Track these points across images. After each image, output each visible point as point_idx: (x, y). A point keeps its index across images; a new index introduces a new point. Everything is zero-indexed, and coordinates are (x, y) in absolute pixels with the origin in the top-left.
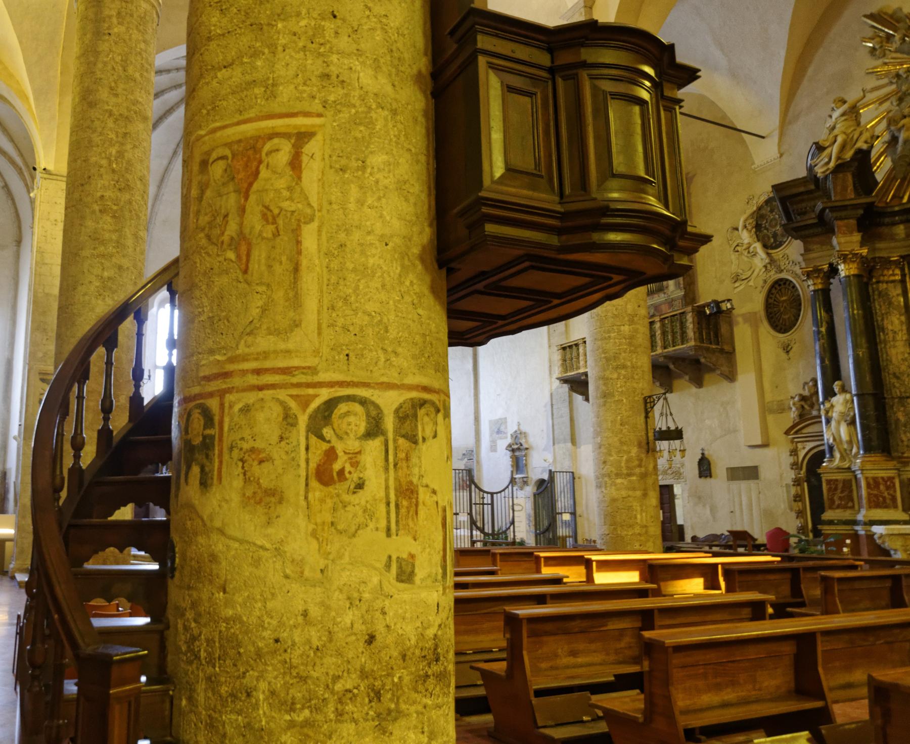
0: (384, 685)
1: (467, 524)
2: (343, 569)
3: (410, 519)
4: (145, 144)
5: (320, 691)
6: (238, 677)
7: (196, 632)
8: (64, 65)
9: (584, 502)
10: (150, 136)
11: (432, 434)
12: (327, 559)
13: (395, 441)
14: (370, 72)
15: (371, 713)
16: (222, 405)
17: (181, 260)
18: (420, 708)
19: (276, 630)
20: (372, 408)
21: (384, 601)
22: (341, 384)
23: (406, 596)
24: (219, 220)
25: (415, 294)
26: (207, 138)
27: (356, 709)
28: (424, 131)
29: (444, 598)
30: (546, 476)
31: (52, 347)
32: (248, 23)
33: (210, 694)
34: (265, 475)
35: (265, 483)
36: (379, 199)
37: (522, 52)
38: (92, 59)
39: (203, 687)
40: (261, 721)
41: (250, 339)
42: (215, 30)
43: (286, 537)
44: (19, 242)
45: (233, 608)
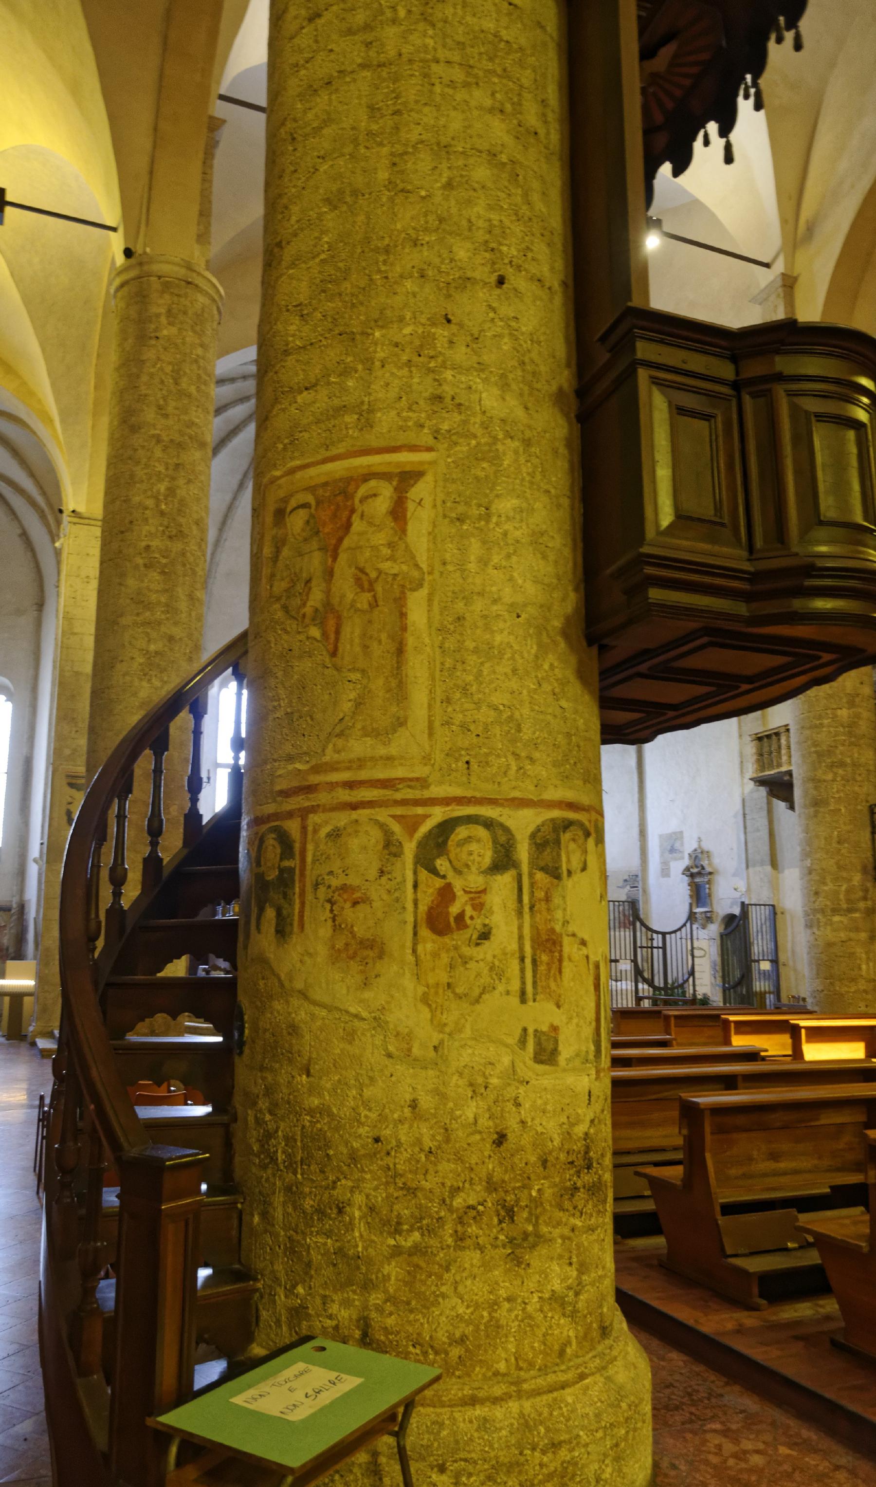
0: (517, 1201)
1: (631, 974)
2: (463, 1046)
3: (552, 979)
4: (202, 478)
5: (434, 1208)
6: (327, 1188)
7: (271, 1126)
8: (99, 377)
9: (789, 945)
10: (209, 467)
11: (581, 865)
12: (441, 1032)
13: (531, 875)
14: (496, 391)
15: (502, 1237)
16: (304, 828)
17: (251, 637)
18: (566, 1231)
19: (375, 1126)
20: (500, 832)
21: (517, 1088)
22: (460, 801)
23: (546, 1082)
24: (299, 587)
25: (557, 680)
26: (283, 480)
27: (481, 1232)
28: (566, 465)
29: (597, 1083)
30: (737, 911)
31: (83, 742)
32: (337, 332)
33: (290, 1210)
34: (361, 921)
35: (360, 931)
36: (508, 556)
37: (697, 362)
38: (134, 370)
39: (282, 1199)
40: (357, 1246)
41: (340, 742)
42: (293, 341)
43: (388, 1003)
44: (40, 605)
45: (320, 1095)
